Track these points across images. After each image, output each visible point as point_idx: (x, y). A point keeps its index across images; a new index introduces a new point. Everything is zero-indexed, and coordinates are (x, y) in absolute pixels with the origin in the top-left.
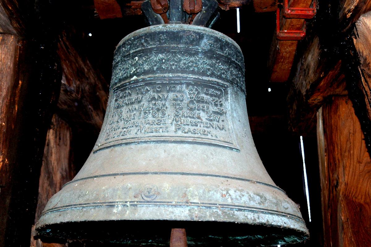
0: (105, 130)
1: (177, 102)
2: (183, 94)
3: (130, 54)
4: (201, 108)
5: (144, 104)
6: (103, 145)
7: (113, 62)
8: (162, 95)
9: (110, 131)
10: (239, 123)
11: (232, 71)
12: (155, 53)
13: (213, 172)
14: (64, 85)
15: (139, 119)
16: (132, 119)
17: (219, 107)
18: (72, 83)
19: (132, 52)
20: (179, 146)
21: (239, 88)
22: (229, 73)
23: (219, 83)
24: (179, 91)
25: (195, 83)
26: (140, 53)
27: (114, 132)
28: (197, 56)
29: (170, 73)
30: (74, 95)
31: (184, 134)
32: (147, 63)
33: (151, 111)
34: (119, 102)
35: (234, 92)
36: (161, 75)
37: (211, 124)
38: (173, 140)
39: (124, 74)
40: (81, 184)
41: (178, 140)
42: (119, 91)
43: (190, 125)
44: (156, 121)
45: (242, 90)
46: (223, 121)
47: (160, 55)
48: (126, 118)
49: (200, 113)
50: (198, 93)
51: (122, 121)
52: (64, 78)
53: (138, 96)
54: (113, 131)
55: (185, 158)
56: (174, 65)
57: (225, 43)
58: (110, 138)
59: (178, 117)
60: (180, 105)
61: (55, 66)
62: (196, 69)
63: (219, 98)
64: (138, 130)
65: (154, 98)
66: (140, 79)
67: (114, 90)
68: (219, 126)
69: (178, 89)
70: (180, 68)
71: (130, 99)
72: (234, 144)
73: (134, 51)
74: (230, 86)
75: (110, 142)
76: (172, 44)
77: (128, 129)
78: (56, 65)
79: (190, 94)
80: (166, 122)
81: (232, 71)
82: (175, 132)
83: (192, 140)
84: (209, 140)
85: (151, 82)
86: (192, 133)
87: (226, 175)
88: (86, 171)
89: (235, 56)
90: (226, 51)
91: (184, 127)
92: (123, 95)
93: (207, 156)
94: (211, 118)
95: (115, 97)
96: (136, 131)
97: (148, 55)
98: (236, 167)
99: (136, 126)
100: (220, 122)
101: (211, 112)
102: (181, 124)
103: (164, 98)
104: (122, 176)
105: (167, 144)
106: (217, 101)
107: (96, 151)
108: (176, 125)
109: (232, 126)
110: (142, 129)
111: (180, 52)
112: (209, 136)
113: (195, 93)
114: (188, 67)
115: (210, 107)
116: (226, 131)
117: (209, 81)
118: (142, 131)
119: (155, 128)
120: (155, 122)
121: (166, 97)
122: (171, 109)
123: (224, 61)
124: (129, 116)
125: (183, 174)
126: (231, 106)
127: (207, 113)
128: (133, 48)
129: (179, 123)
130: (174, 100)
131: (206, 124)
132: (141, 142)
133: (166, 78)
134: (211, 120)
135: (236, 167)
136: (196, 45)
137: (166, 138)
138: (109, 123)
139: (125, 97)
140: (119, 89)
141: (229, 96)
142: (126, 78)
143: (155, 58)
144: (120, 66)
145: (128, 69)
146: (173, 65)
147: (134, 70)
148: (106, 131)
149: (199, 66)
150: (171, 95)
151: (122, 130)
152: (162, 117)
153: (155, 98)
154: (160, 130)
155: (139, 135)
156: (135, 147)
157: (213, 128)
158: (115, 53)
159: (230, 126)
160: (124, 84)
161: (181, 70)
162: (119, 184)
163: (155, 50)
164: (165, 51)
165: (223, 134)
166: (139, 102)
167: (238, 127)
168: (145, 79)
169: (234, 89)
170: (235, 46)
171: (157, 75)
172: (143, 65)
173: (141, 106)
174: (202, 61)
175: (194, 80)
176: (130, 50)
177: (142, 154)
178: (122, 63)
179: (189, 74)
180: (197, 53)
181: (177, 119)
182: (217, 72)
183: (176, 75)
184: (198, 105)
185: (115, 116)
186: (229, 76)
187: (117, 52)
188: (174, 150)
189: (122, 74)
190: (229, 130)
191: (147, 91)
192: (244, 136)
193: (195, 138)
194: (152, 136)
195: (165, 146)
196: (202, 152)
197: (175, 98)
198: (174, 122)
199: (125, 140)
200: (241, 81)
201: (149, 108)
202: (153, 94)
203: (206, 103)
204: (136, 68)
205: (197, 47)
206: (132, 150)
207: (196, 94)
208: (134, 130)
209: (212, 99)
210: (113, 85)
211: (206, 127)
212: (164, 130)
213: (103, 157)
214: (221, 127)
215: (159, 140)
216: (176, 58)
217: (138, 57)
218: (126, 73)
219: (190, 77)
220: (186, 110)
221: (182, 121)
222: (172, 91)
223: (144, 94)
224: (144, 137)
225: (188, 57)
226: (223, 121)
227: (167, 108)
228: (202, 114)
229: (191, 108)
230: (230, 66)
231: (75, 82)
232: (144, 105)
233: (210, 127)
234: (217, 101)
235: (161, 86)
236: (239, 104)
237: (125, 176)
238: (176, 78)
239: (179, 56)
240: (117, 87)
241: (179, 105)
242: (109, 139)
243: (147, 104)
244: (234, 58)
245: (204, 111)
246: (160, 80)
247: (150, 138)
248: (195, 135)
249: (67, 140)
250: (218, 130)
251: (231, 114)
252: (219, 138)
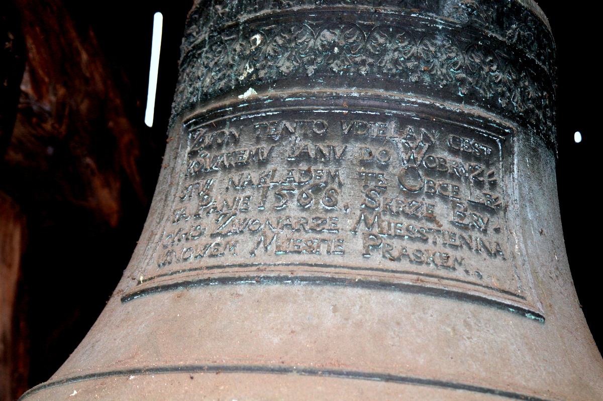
0: (157, 237)
1: (371, 171)
2: (387, 149)
3: (237, 25)
4: (438, 189)
5: (275, 171)
6: (151, 279)
7: (181, 43)
8: (329, 146)
9: (173, 242)
10: (541, 238)
11: (525, 88)
12: (311, 25)
13: (474, 378)
14: (26, 95)
15: (261, 211)
16: (241, 212)
17: (488, 191)
18: (48, 91)
19: (243, 18)
20: (375, 297)
21: (541, 138)
22: (518, 95)
23: (491, 122)
24: (378, 140)
25: (422, 118)
26: (267, 25)
27: (188, 244)
28: (429, 40)
29: (353, 86)
30: (48, 126)
31: (389, 262)
32: (286, 55)
33: (296, 192)
34: (203, 160)
35: (528, 150)
36: (329, 91)
37: (463, 238)
38: (359, 277)
39: (220, 79)
40: (87, 391)
41: (373, 279)
42: (203, 127)
43: (406, 237)
44: (310, 221)
45: (549, 145)
46: (497, 230)
47: (326, 33)
48: (223, 206)
49: (434, 206)
50: (431, 148)
51: (211, 216)
52: (26, 77)
53: (259, 146)
54: (183, 241)
55: (392, 333)
56: (364, 65)
57: (509, 6)
58: (174, 259)
59: (371, 213)
60: (380, 180)
61: (9, 40)
62: (427, 79)
63: (488, 165)
64: (259, 243)
65: (307, 154)
66: (267, 99)
67: (185, 123)
68: (487, 244)
69: (375, 135)
70: (383, 74)
71: (235, 154)
72: (529, 298)
73: (252, 16)
74: (518, 132)
75: (175, 273)
76: (362, 4)
77: (227, 239)
78: (11, 37)
79: (407, 149)
80: (339, 226)
81: (525, 88)
82: (364, 255)
83: (411, 280)
84: (458, 283)
85: (297, 107)
86: (411, 261)
87: (511, 390)
88: (100, 352)
89: (535, 47)
90: (510, 31)
91: (388, 241)
92: (215, 140)
93: (454, 329)
94: (466, 221)
95: (189, 143)
96: (251, 245)
97: (290, 31)
98: (537, 367)
99: (253, 232)
100: (488, 232)
101: (466, 205)
102: (381, 232)
103: (335, 158)
104: (211, 375)
105: (341, 290)
106: (481, 174)
107: (131, 296)
108: (366, 236)
109: (522, 246)
110: (268, 241)
111: (384, 28)
112: (460, 273)
113: (421, 148)
114: (405, 73)
115: (464, 189)
116: (504, 259)
117: (462, 114)
118: (269, 248)
119: (307, 241)
120: (307, 223)
121: (339, 154)
122: (352, 189)
123: (503, 58)
124: (230, 201)
125: (389, 378)
126: (520, 189)
127: (454, 206)
128: (249, 8)
129: (376, 230)
130: (363, 163)
131: (450, 237)
132: (267, 278)
133: (341, 101)
134: (465, 228)
135: (537, 367)
136: (430, 9)
137: (337, 270)
138: (169, 217)
139: (220, 146)
140: (203, 122)
141: (516, 161)
142: (224, 93)
143: (312, 42)
144: (206, 56)
145: (232, 66)
146: (363, 62)
147: (250, 71)
148: (160, 239)
149: (434, 72)
150: (354, 149)
151: (209, 240)
152: (327, 211)
153: (309, 155)
154: (321, 248)
155: (261, 257)
156: (249, 292)
157: (470, 248)
158: (191, 16)
159: (516, 247)
160: (217, 109)
161: (386, 80)
162: (205, 396)
163: (313, 19)
164: (341, 24)
165: (498, 269)
166: (263, 163)
167: (538, 250)
168: (282, 98)
169: (528, 140)
170: (536, 17)
171: (316, 90)
172: (275, 58)
173: (267, 176)
174: (445, 57)
175: (422, 109)
176: (238, 12)
177: (270, 312)
178: (214, 48)
179: (406, 90)
180: (430, 33)
181: (371, 218)
182: (484, 90)
183: (369, 94)
184: (428, 182)
185: (190, 199)
186: (517, 103)
187: (196, 16)
188: (361, 307)
189: (213, 81)
190: (514, 257)
191: (287, 133)
192: (553, 275)
193: (421, 277)
194: (299, 264)
195: (334, 293)
196: (439, 318)
197: (366, 157)
198: (362, 226)
199: (220, 270)
200: (548, 117)
201: (290, 182)
202: (303, 143)
203: (452, 175)
204: (255, 66)
205: (431, 14)
206: (240, 298)
207: (424, 151)
208: (246, 242)
209: (470, 166)
210: (184, 109)
211: (450, 245)
212: (333, 249)
213: (153, 313)
214: (493, 248)
215: (319, 275)
216: (371, 45)
217: (262, 34)
218: (224, 78)
219: (409, 102)
220: (396, 194)
221: (385, 224)
222: (357, 138)
223: (275, 142)
224: (275, 265)
225: (406, 43)
226: (497, 230)
227: (340, 185)
228: (441, 209)
229: (410, 190)
230: (520, 73)
231: (55, 89)
232: (277, 174)
233: (461, 246)
234: (481, 174)
235: (325, 123)
236: (540, 184)
237: (222, 376)
238: (372, 103)
239: (379, 38)
240: (196, 117)
241: (375, 178)
242: (170, 263)
243: (286, 172)
244: (531, 51)
245: (444, 198)
246: (322, 105)
247: (291, 268)
248: (419, 267)
249: (12, 249)
250: (485, 255)
251: (519, 213)
252: (486, 280)
